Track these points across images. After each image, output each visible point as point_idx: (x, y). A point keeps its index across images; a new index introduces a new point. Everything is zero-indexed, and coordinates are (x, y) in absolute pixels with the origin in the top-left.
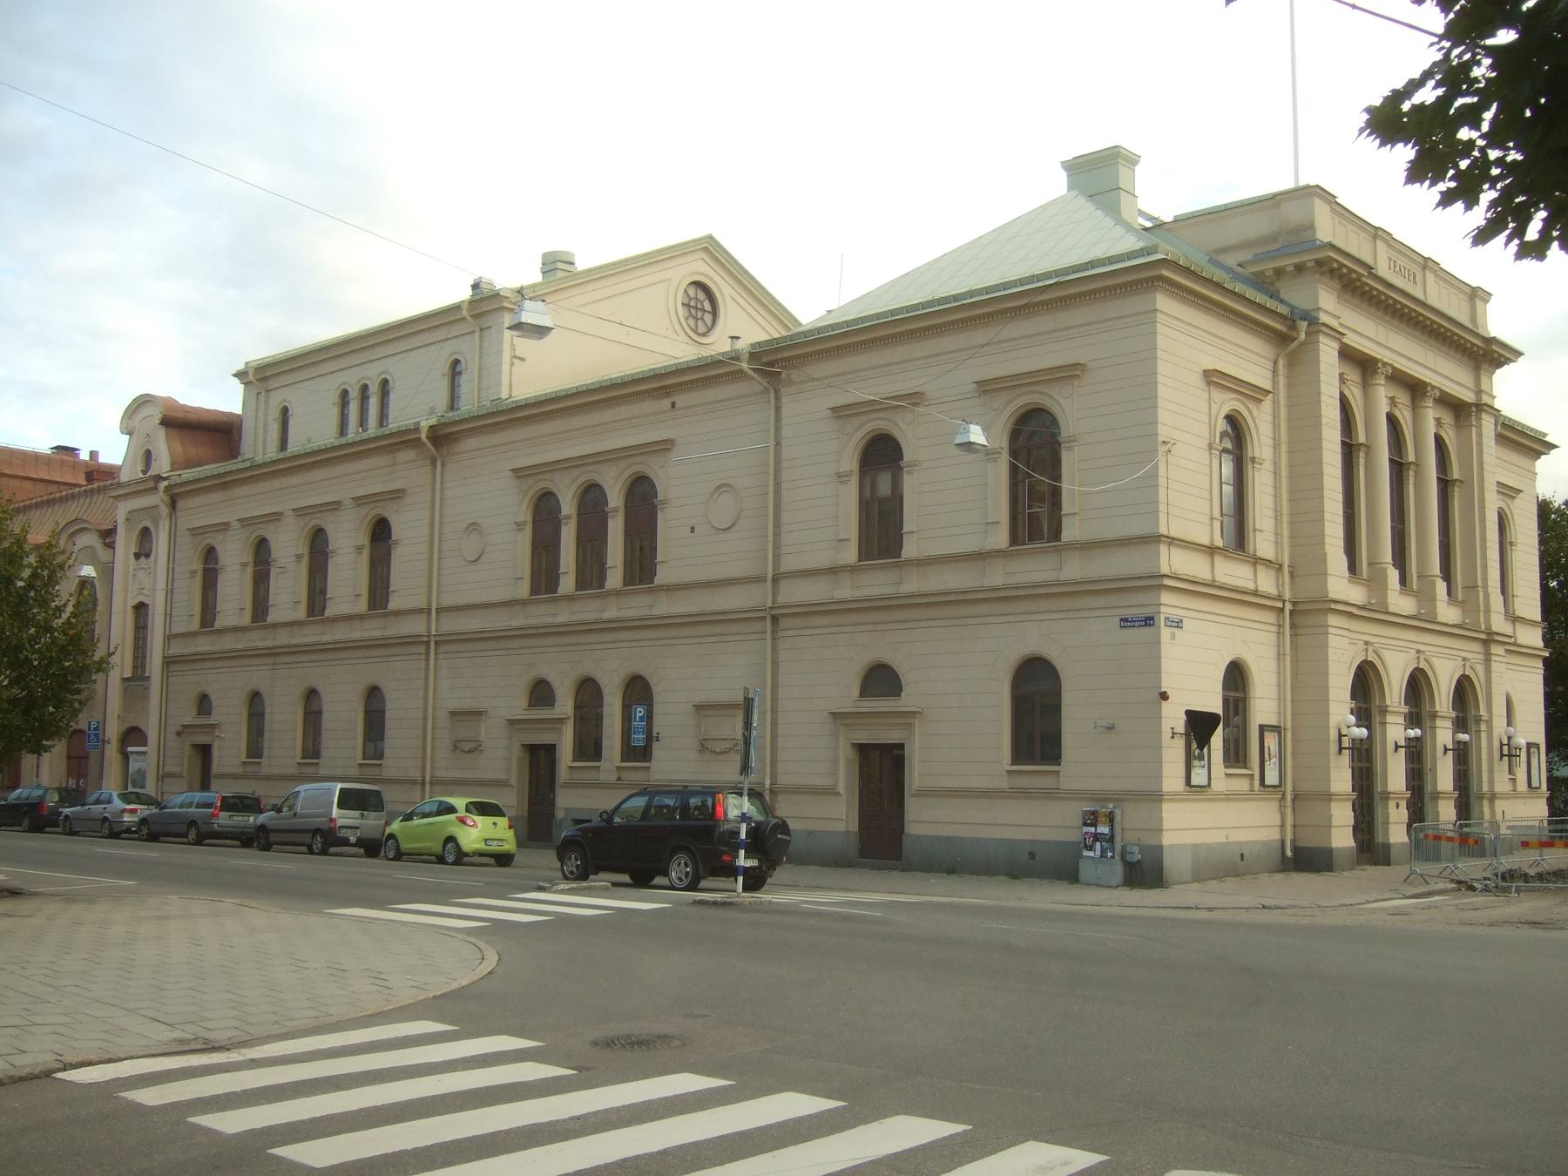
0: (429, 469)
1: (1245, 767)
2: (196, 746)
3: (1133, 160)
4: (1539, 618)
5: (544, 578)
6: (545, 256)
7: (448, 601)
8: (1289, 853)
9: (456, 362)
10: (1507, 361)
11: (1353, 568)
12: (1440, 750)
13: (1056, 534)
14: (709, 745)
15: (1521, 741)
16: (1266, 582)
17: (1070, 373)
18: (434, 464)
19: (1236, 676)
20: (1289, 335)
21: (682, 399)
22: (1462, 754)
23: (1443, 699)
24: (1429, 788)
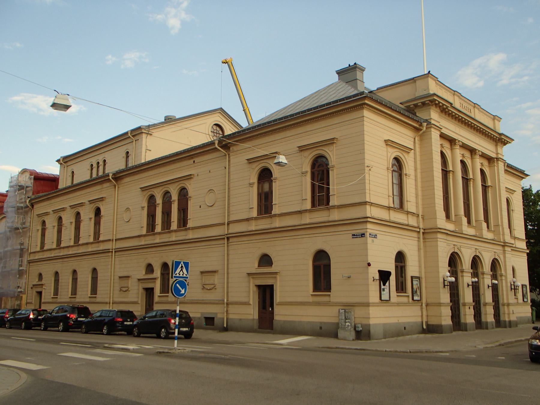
0: (113, 189)
1: (406, 293)
2: (37, 292)
3: (363, 70)
4: (525, 238)
5: (151, 226)
6: (166, 117)
7: (118, 237)
8: (425, 327)
9: (128, 153)
10: (508, 142)
11: (448, 217)
12: (486, 287)
13: (328, 203)
14: (205, 286)
15: (519, 284)
16: (412, 221)
17: (331, 142)
18: (115, 186)
19: (400, 257)
20: (420, 128)
21: (197, 160)
22: (495, 289)
23: (487, 266)
24: (482, 302)
